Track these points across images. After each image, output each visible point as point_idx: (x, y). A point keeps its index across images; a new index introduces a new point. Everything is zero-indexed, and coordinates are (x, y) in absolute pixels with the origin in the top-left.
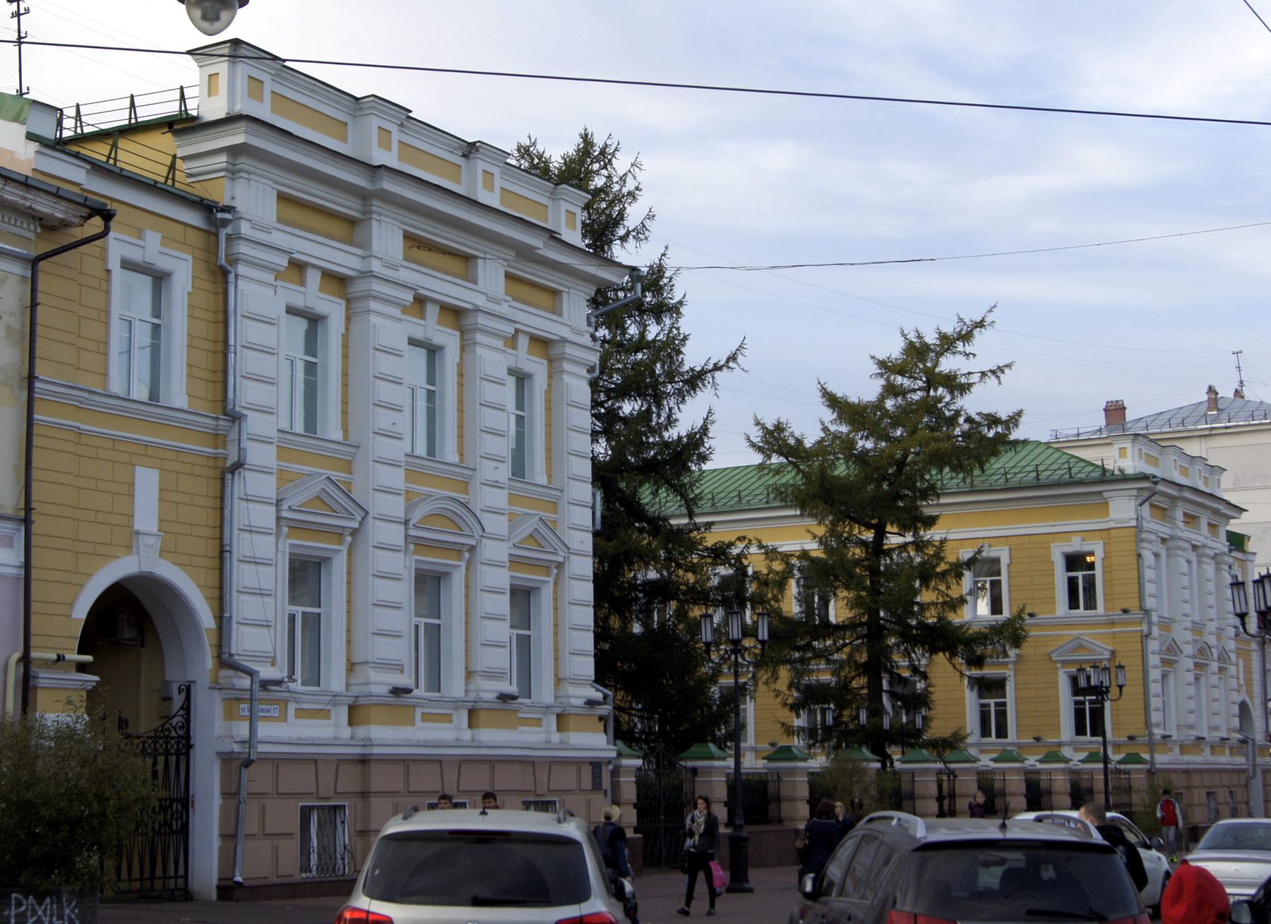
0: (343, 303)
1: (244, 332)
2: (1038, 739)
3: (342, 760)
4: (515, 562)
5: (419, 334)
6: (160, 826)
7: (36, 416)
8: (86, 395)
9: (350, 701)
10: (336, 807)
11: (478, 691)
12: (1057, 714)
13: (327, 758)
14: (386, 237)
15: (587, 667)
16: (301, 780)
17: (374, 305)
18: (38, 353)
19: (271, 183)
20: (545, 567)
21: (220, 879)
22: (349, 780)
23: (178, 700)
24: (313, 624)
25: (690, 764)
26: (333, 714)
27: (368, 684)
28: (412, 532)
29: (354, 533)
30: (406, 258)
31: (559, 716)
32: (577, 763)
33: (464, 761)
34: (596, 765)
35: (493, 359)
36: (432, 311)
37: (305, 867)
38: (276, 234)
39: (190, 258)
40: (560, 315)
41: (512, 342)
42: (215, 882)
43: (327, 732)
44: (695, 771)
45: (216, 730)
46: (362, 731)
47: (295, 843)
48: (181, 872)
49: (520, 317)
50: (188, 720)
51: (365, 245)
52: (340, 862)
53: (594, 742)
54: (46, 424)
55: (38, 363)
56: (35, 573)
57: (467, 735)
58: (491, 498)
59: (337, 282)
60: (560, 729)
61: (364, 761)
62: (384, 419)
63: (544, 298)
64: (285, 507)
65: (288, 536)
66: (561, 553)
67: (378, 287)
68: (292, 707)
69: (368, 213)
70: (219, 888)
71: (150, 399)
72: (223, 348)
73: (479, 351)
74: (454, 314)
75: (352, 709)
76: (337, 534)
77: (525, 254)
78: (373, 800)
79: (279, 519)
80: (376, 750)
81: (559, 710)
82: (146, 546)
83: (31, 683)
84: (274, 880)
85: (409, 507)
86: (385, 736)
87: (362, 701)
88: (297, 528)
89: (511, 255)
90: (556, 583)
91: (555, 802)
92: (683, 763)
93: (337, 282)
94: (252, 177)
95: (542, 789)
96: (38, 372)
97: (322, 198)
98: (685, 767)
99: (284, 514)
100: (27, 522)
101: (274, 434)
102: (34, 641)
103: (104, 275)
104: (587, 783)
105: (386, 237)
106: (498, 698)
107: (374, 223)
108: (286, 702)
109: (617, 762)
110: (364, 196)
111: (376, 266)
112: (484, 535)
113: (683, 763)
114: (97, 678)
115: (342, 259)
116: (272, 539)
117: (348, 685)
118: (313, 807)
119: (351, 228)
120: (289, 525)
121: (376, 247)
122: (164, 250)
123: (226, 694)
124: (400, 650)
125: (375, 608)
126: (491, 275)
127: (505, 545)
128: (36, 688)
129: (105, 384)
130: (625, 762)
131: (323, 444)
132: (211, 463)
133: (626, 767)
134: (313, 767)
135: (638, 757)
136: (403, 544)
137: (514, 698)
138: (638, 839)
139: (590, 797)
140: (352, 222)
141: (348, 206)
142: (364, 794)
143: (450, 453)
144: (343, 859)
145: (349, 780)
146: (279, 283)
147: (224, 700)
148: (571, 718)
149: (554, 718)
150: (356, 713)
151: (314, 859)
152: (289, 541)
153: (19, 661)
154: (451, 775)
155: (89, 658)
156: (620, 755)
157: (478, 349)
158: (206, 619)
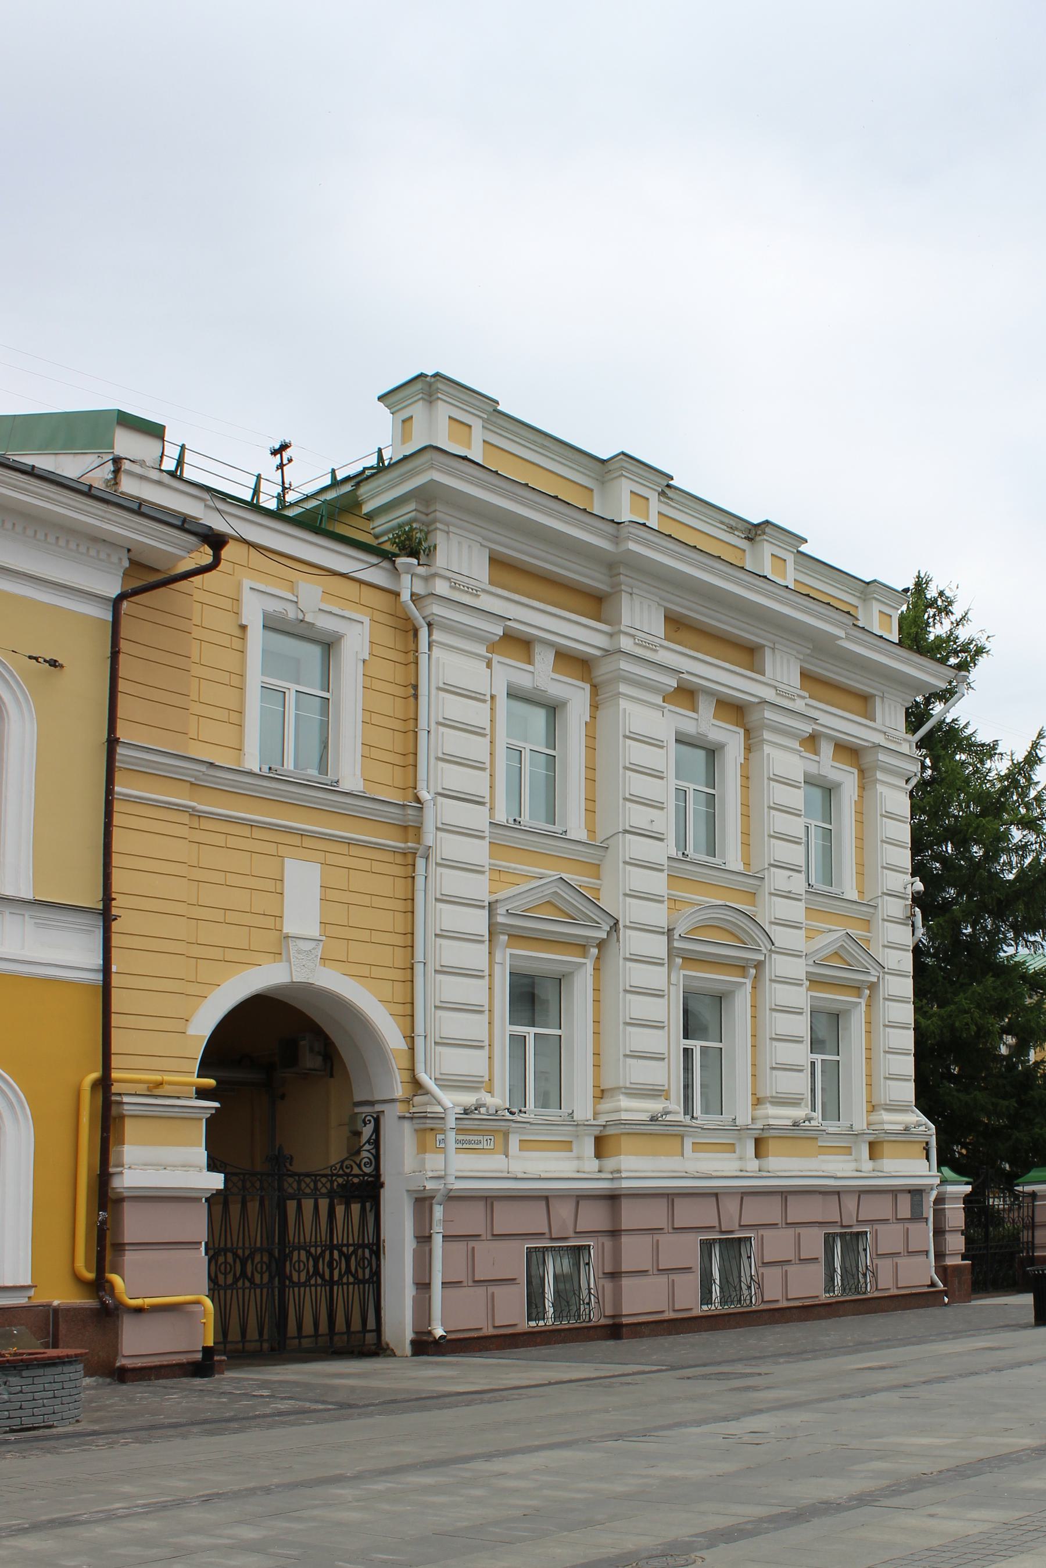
0: (587, 687)
1: (436, 706)
3: (580, 1198)
4: (815, 982)
5: (689, 727)
6: (341, 1276)
7: (117, 789)
8: (203, 768)
9: (596, 1131)
11: (767, 1117)
13: (730, 1192)
15: (907, 1091)
17: (623, 688)
18: (120, 713)
19: (657, 599)
20: (741, 968)
21: (416, 1333)
22: (594, 1218)
23: (367, 1131)
24: (833, 1070)
25: (1028, 1189)
26: (575, 1146)
27: (882, 1123)
29: (601, 944)
30: (491, 583)
31: (871, 1145)
32: (894, 1192)
33: (745, 1194)
34: (916, 1193)
35: (784, 760)
36: (706, 708)
38: (484, 597)
39: (366, 620)
40: (873, 719)
41: (812, 741)
42: (409, 1335)
43: (726, 1167)
44: (1033, 1195)
45: (407, 1164)
46: (610, 1163)
47: (820, 1269)
48: (371, 1324)
49: (824, 719)
50: (377, 1157)
51: (613, 620)
52: (745, 1292)
53: (918, 1169)
54: (128, 799)
55: (120, 725)
56: (115, 980)
58: (782, 910)
59: (576, 663)
61: (613, 1199)
62: (639, 817)
64: (501, 911)
65: (682, 968)
66: (873, 972)
67: (624, 665)
68: (514, 1142)
70: (413, 1343)
72: (410, 727)
73: (767, 749)
74: (734, 710)
75: (599, 1141)
76: (582, 948)
78: (625, 1239)
80: (625, 1184)
81: (871, 1138)
82: (299, 952)
83: (114, 1111)
86: (638, 1167)
87: (610, 1131)
88: (691, 960)
90: (868, 1006)
91: (866, 1232)
92: (1020, 1188)
93: (576, 663)
94: (452, 529)
95: (849, 1219)
96: (121, 733)
97: (546, 561)
98: (1023, 1192)
100: (107, 916)
101: (665, 862)
102: (115, 1061)
103: (237, 632)
104: (905, 1211)
105: (641, 617)
107: (625, 597)
108: (506, 1135)
109: (942, 1188)
110: (612, 565)
111: (626, 643)
112: (774, 950)
113: (1020, 1188)
114: (217, 1105)
116: (665, 969)
118: (545, 1249)
119: (596, 603)
120: (680, 956)
121: (626, 620)
123: (418, 1124)
124: (798, 1084)
125: (628, 1025)
126: (782, 671)
127: (802, 961)
128: (122, 1117)
129: (239, 760)
130: (950, 1189)
132: (399, 859)
133: (952, 1193)
134: (714, 1199)
135: (967, 1183)
138: (965, 1265)
139: (907, 1225)
141: (593, 579)
142: (615, 1233)
143: (733, 858)
144: (749, 1288)
145: (594, 1218)
146: (496, 658)
147: (416, 1131)
148: (885, 1145)
150: (601, 1146)
153: (95, 1085)
154: (731, 1207)
155: (211, 1082)
156: (944, 1182)
157: (765, 747)
158: (392, 1037)
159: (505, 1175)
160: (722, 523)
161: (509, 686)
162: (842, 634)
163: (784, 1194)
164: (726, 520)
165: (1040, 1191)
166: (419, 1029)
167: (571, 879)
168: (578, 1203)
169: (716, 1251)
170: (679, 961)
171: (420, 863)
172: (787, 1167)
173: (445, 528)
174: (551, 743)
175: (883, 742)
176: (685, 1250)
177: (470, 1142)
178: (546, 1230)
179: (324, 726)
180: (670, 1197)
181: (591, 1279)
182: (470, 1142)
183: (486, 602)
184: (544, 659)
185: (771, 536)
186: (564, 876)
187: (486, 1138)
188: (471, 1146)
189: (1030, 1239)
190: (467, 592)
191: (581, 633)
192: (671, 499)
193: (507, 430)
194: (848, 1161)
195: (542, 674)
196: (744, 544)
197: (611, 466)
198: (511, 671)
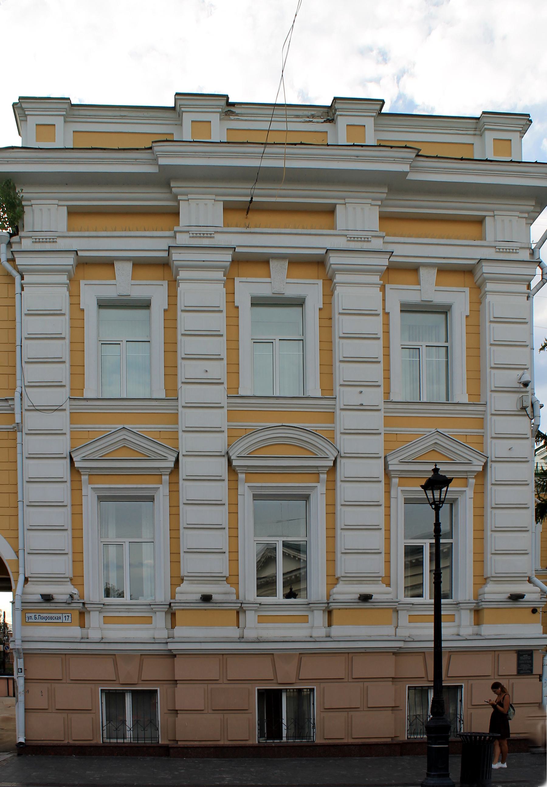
14: (201, 211)
16: (104, 670)
26: (310, 618)
32: (496, 652)
39: (467, 290)
57: (320, 632)
60: (478, 622)
63: (472, 229)
66: (475, 462)
71: (166, 397)
73: (489, 298)
76: (156, 474)
77: (396, 184)
86: (191, 634)
89: (382, 192)
94: (496, 213)
105: (201, 211)
106: (359, 598)
115: (149, 242)
122: (134, 282)
131: (458, 408)
148: (485, 611)
152: (400, 488)
159: (393, 638)
160: (297, 116)
161: (402, 305)
162: (406, 168)
163: (350, 654)
164: (306, 113)
166: (21, 546)
167: (308, 427)
171: (19, 434)
172: (352, 632)
173: (491, 213)
177: (51, 618)
178: (424, 675)
179: (447, 362)
182: (51, 618)
184: (428, 276)
185: (343, 109)
186: (126, 426)
187: (64, 615)
188: (52, 621)
190: (43, 242)
191: (149, 242)
192: (242, 114)
193: (95, 116)
194: (147, 629)
195: (124, 282)
196: (327, 127)
197: (483, 120)
198: (400, 293)
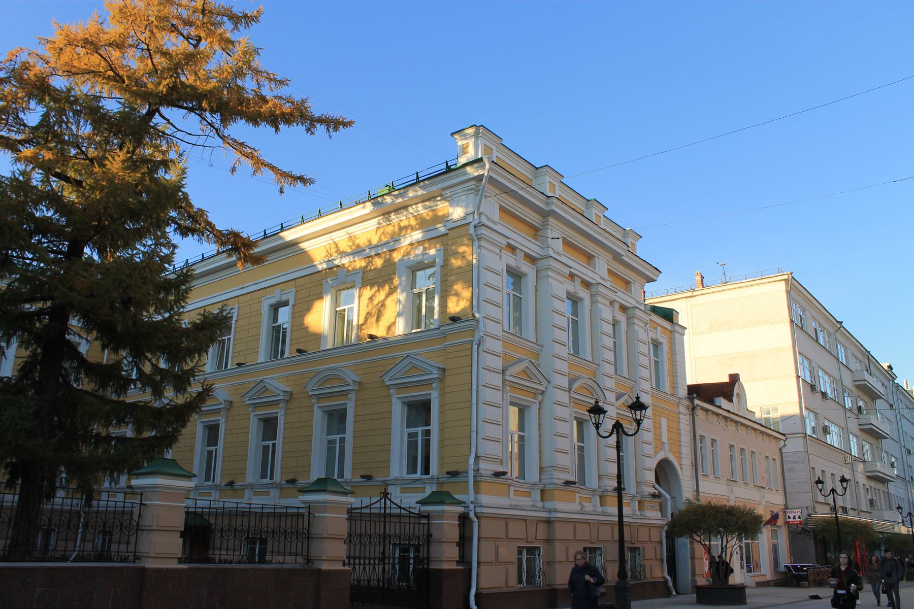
2: (369, 478)
10: (595, 549)
12: (386, 448)
16: (517, 530)
20: (535, 393)
22: (542, 532)
26: (532, 494)
28: (572, 395)
36: (578, 282)
37: (520, 582)
46: (549, 505)
61: (549, 522)
64: (508, 373)
65: (510, 391)
69: (545, 225)
74: (587, 284)
79: (504, 380)
80: (559, 515)
84: (505, 590)
85: (571, 382)
87: (548, 487)
99: (508, 378)
115: (533, 247)
117: (540, 480)
118: (523, 547)
126: (602, 264)
136: (501, 385)
137: (574, 483)
140: (536, 230)
149: (598, 498)
150: (544, 494)
151: (524, 578)
165: (435, 512)
168: (507, 524)
169: (525, 552)
170: (508, 388)
174: (656, 355)
175: (602, 282)
176: (508, 552)
180: (507, 519)
181: (539, 564)
183: (498, 228)
189: (426, 555)
197: (590, 203)
